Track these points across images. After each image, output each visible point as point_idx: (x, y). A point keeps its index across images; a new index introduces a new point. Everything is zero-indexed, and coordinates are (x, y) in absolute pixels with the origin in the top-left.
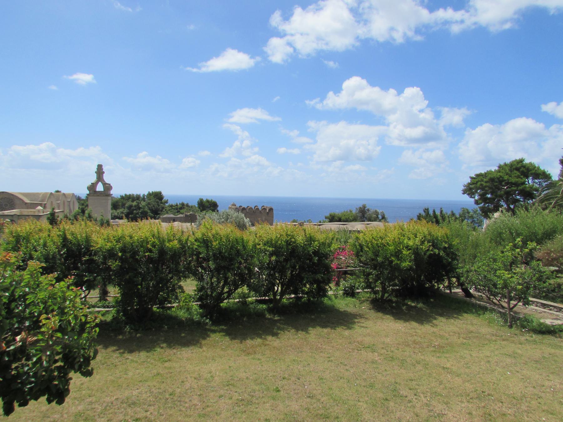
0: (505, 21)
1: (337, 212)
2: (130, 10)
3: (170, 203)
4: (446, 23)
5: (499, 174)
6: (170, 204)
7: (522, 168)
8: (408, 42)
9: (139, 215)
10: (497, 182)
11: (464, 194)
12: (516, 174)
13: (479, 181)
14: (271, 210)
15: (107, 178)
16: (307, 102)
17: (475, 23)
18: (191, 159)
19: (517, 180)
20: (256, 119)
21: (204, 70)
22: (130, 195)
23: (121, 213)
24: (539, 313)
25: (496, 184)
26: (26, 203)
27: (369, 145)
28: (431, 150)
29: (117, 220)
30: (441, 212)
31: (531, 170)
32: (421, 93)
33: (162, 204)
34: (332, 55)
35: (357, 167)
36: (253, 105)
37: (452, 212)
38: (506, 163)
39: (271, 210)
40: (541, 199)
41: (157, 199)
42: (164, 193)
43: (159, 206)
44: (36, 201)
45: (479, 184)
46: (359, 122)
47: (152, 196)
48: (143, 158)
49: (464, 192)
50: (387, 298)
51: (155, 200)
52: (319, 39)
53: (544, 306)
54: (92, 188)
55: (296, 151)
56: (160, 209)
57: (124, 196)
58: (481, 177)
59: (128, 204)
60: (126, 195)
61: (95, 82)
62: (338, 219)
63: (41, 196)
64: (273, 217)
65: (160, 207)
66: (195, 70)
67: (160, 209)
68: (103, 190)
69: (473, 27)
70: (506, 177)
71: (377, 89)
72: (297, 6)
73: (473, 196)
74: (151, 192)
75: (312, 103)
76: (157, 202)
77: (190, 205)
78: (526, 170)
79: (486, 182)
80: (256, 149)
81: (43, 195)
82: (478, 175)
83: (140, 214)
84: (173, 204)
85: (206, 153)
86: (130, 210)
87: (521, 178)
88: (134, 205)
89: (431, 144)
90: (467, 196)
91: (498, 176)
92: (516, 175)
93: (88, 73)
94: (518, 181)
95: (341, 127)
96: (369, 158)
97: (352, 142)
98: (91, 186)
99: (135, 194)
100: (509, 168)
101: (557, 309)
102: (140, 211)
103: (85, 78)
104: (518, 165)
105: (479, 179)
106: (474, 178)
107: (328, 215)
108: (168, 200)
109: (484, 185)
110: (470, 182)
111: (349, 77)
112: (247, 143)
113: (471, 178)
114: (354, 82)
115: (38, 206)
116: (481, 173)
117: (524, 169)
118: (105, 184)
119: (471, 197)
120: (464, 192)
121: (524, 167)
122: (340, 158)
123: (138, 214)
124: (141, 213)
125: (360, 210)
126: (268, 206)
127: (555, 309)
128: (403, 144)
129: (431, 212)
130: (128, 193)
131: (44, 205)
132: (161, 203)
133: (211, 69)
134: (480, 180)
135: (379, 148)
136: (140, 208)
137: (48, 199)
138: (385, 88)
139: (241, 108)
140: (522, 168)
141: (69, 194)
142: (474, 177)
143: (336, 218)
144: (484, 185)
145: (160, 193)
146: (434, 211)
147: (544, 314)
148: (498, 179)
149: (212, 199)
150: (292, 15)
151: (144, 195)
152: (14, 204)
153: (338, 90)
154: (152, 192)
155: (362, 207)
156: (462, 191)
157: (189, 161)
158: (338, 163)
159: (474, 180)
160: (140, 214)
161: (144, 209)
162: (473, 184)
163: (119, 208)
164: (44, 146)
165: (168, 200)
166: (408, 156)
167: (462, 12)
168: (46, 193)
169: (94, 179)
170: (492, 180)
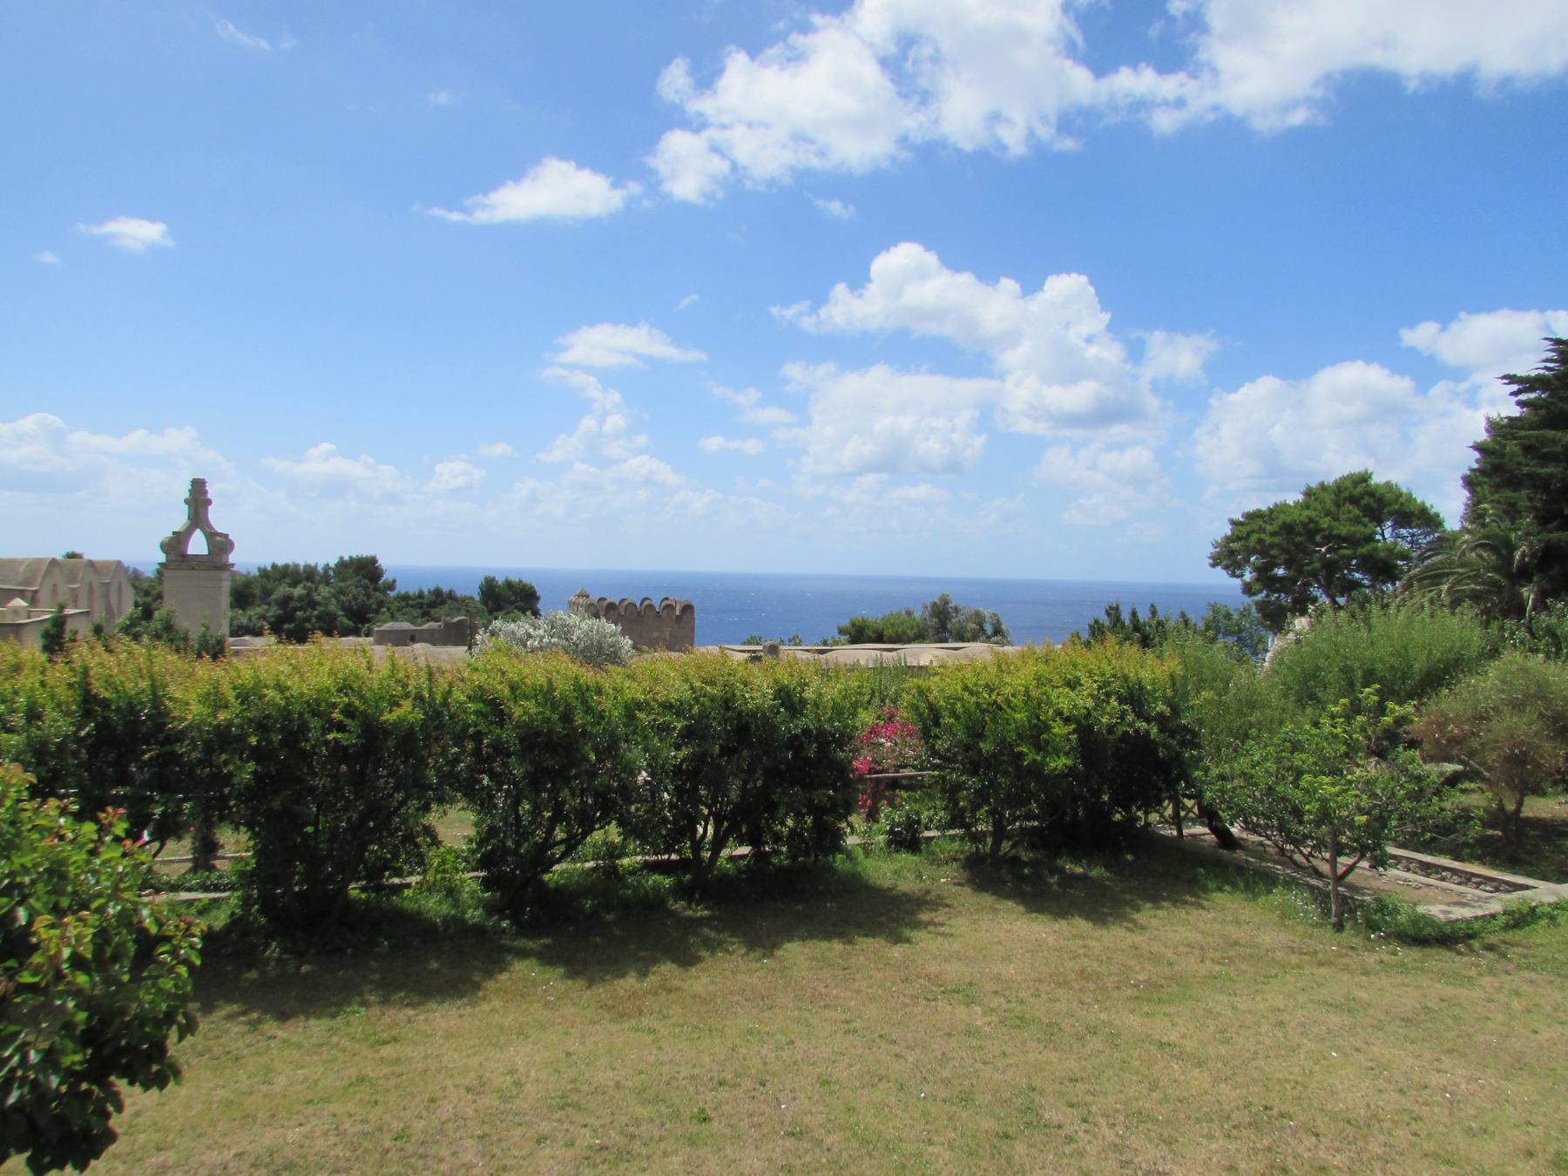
1: (873, 615)
2: (264, 45)
3: (401, 588)
4: (1141, 105)
5: (1307, 512)
6: (403, 592)
7: (1366, 497)
11: (1214, 565)
12: (1350, 512)
13: (1253, 531)
14: (688, 609)
15: (217, 518)
16: (775, 311)
17: (1215, 108)
18: (458, 466)
19: (1353, 529)
20: (639, 356)
21: (482, 217)
22: (287, 566)
23: (259, 618)
24: (1415, 888)
28: (1122, 447)
31: (1389, 504)
32: (1091, 290)
33: (378, 594)
34: (838, 183)
35: (922, 491)
39: (688, 609)
42: (384, 562)
43: (368, 596)
45: (1254, 537)
47: (350, 571)
48: (322, 462)
51: (360, 580)
52: (799, 138)
54: (175, 546)
55: (752, 446)
57: (269, 568)
59: (283, 590)
60: (274, 566)
61: (170, 243)
63: (22, 569)
64: (693, 630)
65: (372, 601)
66: (455, 217)
69: (1211, 117)
71: (966, 279)
73: (1238, 572)
74: (346, 558)
75: (790, 313)
77: (459, 593)
79: (1273, 534)
80: (641, 440)
83: (314, 620)
84: (411, 593)
85: (501, 449)
86: (284, 609)
89: (1120, 431)
91: (1304, 519)
92: (1351, 515)
94: (1355, 533)
95: (875, 381)
96: (953, 467)
97: (907, 423)
98: (171, 540)
100: (1333, 496)
101: (1461, 877)
102: (316, 612)
103: (141, 232)
104: (1355, 487)
108: (394, 581)
110: (1229, 533)
111: (886, 244)
112: (615, 421)
113: (1234, 523)
116: (1259, 511)
117: (1371, 501)
118: (211, 535)
119: (1233, 575)
123: (308, 619)
126: (678, 598)
128: (1041, 429)
129: (1126, 617)
132: (376, 589)
133: (501, 215)
138: (989, 276)
140: (1366, 497)
143: (869, 632)
145: (373, 561)
147: (1426, 890)
150: (720, 72)
151: (328, 565)
153: (859, 280)
154: (351, 558)
157: (452, 472)
158: (870, 480)
159: (1241, 528)
160: (314, 620)
161: (326, 605)
162: (1239, 539)
164: (28, 424)
165: (394, 581)
166: (1059, 463)
167: (1181, 77)
168: (40, 561)
169: (179, 519)
170: (1288, 529)
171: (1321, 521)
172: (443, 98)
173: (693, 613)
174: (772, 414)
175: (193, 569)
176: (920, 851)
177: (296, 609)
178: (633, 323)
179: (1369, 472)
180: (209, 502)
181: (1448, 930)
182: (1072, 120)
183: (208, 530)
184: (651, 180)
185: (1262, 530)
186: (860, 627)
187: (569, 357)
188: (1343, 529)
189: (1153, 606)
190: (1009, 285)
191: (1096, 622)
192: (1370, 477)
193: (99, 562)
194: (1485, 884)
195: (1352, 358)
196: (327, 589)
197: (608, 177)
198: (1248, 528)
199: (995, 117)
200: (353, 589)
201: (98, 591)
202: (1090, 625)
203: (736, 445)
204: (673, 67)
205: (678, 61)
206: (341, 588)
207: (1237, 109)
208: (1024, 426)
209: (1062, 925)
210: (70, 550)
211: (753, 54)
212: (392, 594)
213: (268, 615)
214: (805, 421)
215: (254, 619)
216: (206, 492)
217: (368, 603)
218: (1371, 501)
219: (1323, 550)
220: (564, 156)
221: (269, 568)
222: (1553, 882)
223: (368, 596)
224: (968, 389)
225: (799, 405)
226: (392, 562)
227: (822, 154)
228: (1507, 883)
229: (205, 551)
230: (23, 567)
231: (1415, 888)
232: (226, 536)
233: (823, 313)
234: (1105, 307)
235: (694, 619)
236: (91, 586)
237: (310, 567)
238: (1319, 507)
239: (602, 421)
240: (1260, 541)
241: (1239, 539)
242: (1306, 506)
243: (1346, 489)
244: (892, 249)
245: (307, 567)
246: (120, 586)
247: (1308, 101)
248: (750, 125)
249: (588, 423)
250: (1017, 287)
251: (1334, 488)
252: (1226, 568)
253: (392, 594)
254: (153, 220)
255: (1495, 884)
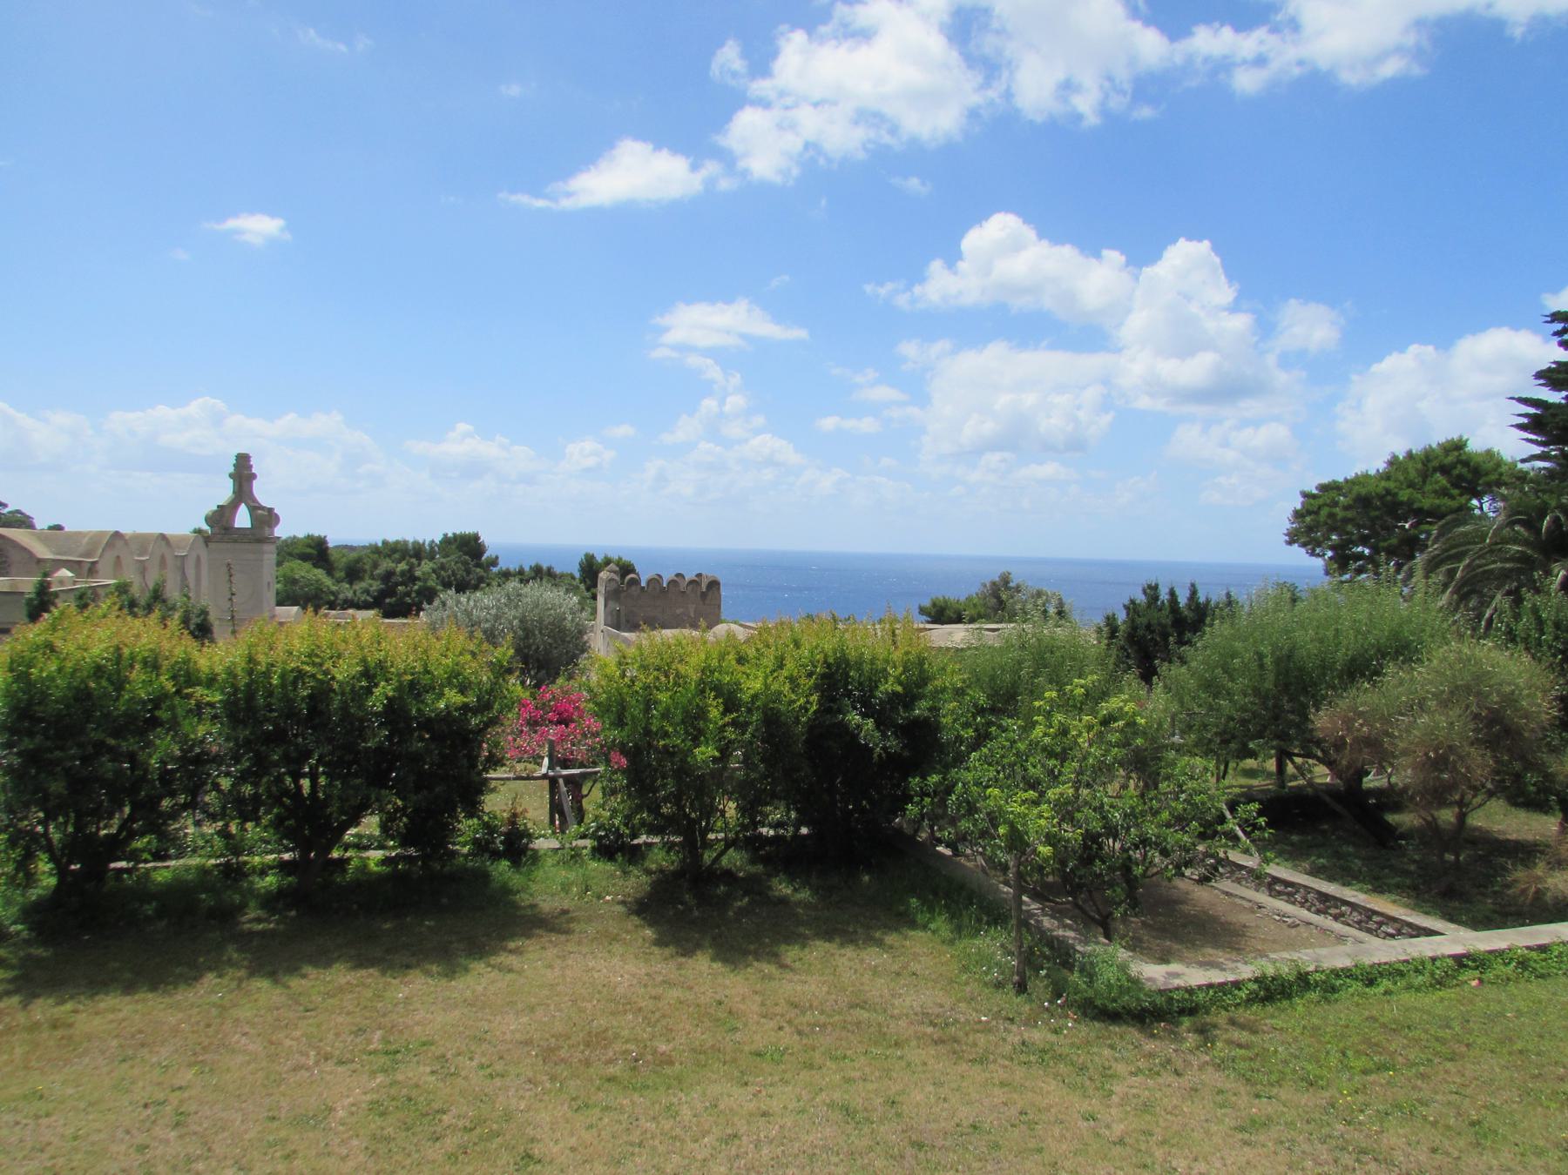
0: (1381, 57)
1: (958, 593)
2: (343, 48)
3: (503, 565)
4: (1223, 66)
5: (1383, 484)
6: (504, 569)
7: (1459, 466)
8: (1112, 121)
9: (413, 599)
10: (1377, 508)
11: (1290, 543)
12: (1437, 482)
13: (1325, 505)
14: (714, 584)
15: (263, 492)
16: (868, 288)
17: (1300, 63)
18: (589, 445)
19: (1437, 502)
20: (743, 336)
21: (566, 204)
22: (397, 542)
23: (362, 593)
24: (1289, 926)
25: (1377, 513)
26: (39, 561)
27: (1079, 408)
28: (1256, 423)
29: (351, 611)
30: (1194, 592)
31: (1487, 474)
32: (1217, 260)
33: (478, 570)
34: (916, 157)
35: (1049, 469)
36: (721, 294)
37: (1228, 595)
38: (1414, 452)
39: (714, 584)
40: (1434, 558)
41: (466, 554)
42: (485, 538)
43: (468, 572)
44: (70, 555)
45: (1325, 512)
46: (1045, 343)
47: (454, 547)
48: (461, 443)
49: (1292, 538)
50: (292, 850)
51: (460, 557)
52: (867, 116)
53: (1325, 903)
54: (221, 518)
55: (867, 425)
56: (473, 582)
57: (380, 544)
58: (1333, 494)
59: (386, 565)
60: (385, 543)
61: (288, 237)
62: (954, 616)
63: (86, 540)
64: (719, 606)
65: (471, 576)
66: (540, 203)
67: (473, 582)
68: (249, 526)
69: (1296, 71)
70: (1404, 495)
71: (1067, 251)
72: (784, 28)
73: (1318, 550)
74: (450, 535)
75: (883, 291)
76: (465, 563)
77: (558, 570)
78: (1469, 471)
79: (1346, 508)
80: (759, 420)
81: (91, 538)
82: (1324, 488)
83: (413, 595)
84: (512, 569)
85: (625, 430)
86: (386, 584)
87: (1452, 497)
88: (398, 570)
89: (1251, 407)
90: (1303, 550)
91: (1380, 490)
92: (1437, 487)
93: (272, 214)
94: (1439, 506)
95: (994, 358)
96: (1075, 446)
97: (1030, 399)
98: (215, 512)
99: (411, 540)
100: (1420, 466)
101: (1361, 914)
102: (416, 587)
103: (260, 227)
104: (1447, 455)
105: (1326, 498)
106: (1314, 497)
107: (927, 603)
108: (497, 558)
109: (1339, 517)
110: (1299, 507)
111: (979, 216)
112: (735, 402)
113: (1305, 495)
114: (1000, 227)
115: (58, 569)
116: (1335, 482)
117: (1464, 471)
118: (255, 508)
119: (1313, 554)
120: (1292, 538)
121: (1466, 464)
122: (994, 445)
123: (408, 594)
124: (419, 592)
125: (992, 589)
126: (709, 573)
127: (1355, 914)
128: (1160, 405)
129: (1164, 596)
130: (393, 537)
131: (86, 567)
132: (478, 565)
133: (584, 201)
134: (1328, 501)
135: (1107, 419)
136: (414, 579)
137: (103, 550)
138: (1091, 247)
139: (689, 301)
140: (1459, 466)
141: (142, 542)
142: (1315, 491)
143: (949, 613)
144: (1339, 517)
145: (476, 537)
146: (1172, 593)
147: (1302, 929)
148: (1381, 497)
149: (621, 555)
150: (774, 54)
151: (433, 541)
152: (5, 562)
153: (952, 257)
154: (454, 534)
155: (997, 579)
156: (1286, 535)
157: (583, 451)
158: (993, 458)
159: (1312, 501)
160: (413, 595)
161: (425, 581)
162: (1309, 513)
163: (361, 579)
164: (194, 408)
165: (497, 558)
166: (1190, 439)
167: (1261, 33)
168: (102, 533)
169: (224, 492)
170: (1364, 502)
171: (1401, 493)
172: (515, 90)
173: (719, 589)
174: (884, 393)
175: (235, 541)
176: (615, 861)
177: (397, 584)
178: (729, 300)
179: (1465, 438)
180: (254, 476)
181: (1160, 1000)
182: (1148, 86)
183: (252, 504)
184: (728, 160)
185: (1335, 504)
186: (941, 607)
187: (672, 337)
188: (1427, 503)
189: (1193, 585)
190: (1114, 257)
191: (1132, 602)
192: (1465, 445)
193: (172, 536)
194: (1387, 924)
195: (1498, 324)
196: (431, 565)
197: (688, 157)
198: (1321, 501)
199: (1068, 87)
200: (453, 561)
201: (170, 562)
202: (1124, 606)
203: (850, 424)
204: (726, 49)
205: (731, 43)
206: (442, 563)
207: (1323, 65)
208: (1144, 403)
209: (186, 996)
210: (52, 523)
211: (810, 30)
212: (495, 570)
213: (371, 589)
214: (923, 400)
215: (358, 593)
216: (251, 467)
217: (467, 579)
218: (1464, 471)
219: (1407, 526)
220: (639, 136)
221: (380, 544)
222: (1529, 925)
223: (468, 572)
224: (1092, 363)
225: (917, 387)
226: (493, 541)
227: (893, 131)
228: (1410, 925)
229: (249, 525)
230: (86, 539)
231: (1289, 926)
232: (270, 510)
233: (917, 290)
234: (1230, 277)
235: (720, 596)
236: (163, 558)
237: (419, 543)
238: (1402, 478)
239: (722, 402)
240: (1332, 515)
241: (1309, 513)
242: (1386, 476)
243: (1436, 458)
244: (984, 223)
245: (416, 543)
246: (198, 559)
247: (1399, 50)
248: (816, 105)
249: (709, 404)
250: (1123, 258)
251: (1422, 457)
252: (1304, 545)
253: (495, 570)
254: (272, 215)
255: (1397, 925)
